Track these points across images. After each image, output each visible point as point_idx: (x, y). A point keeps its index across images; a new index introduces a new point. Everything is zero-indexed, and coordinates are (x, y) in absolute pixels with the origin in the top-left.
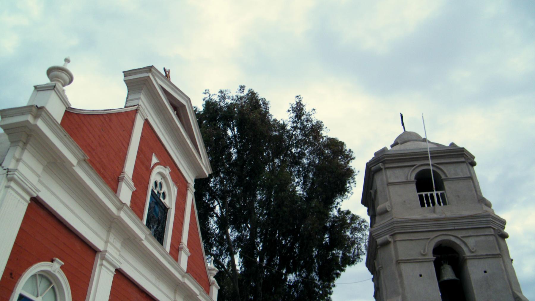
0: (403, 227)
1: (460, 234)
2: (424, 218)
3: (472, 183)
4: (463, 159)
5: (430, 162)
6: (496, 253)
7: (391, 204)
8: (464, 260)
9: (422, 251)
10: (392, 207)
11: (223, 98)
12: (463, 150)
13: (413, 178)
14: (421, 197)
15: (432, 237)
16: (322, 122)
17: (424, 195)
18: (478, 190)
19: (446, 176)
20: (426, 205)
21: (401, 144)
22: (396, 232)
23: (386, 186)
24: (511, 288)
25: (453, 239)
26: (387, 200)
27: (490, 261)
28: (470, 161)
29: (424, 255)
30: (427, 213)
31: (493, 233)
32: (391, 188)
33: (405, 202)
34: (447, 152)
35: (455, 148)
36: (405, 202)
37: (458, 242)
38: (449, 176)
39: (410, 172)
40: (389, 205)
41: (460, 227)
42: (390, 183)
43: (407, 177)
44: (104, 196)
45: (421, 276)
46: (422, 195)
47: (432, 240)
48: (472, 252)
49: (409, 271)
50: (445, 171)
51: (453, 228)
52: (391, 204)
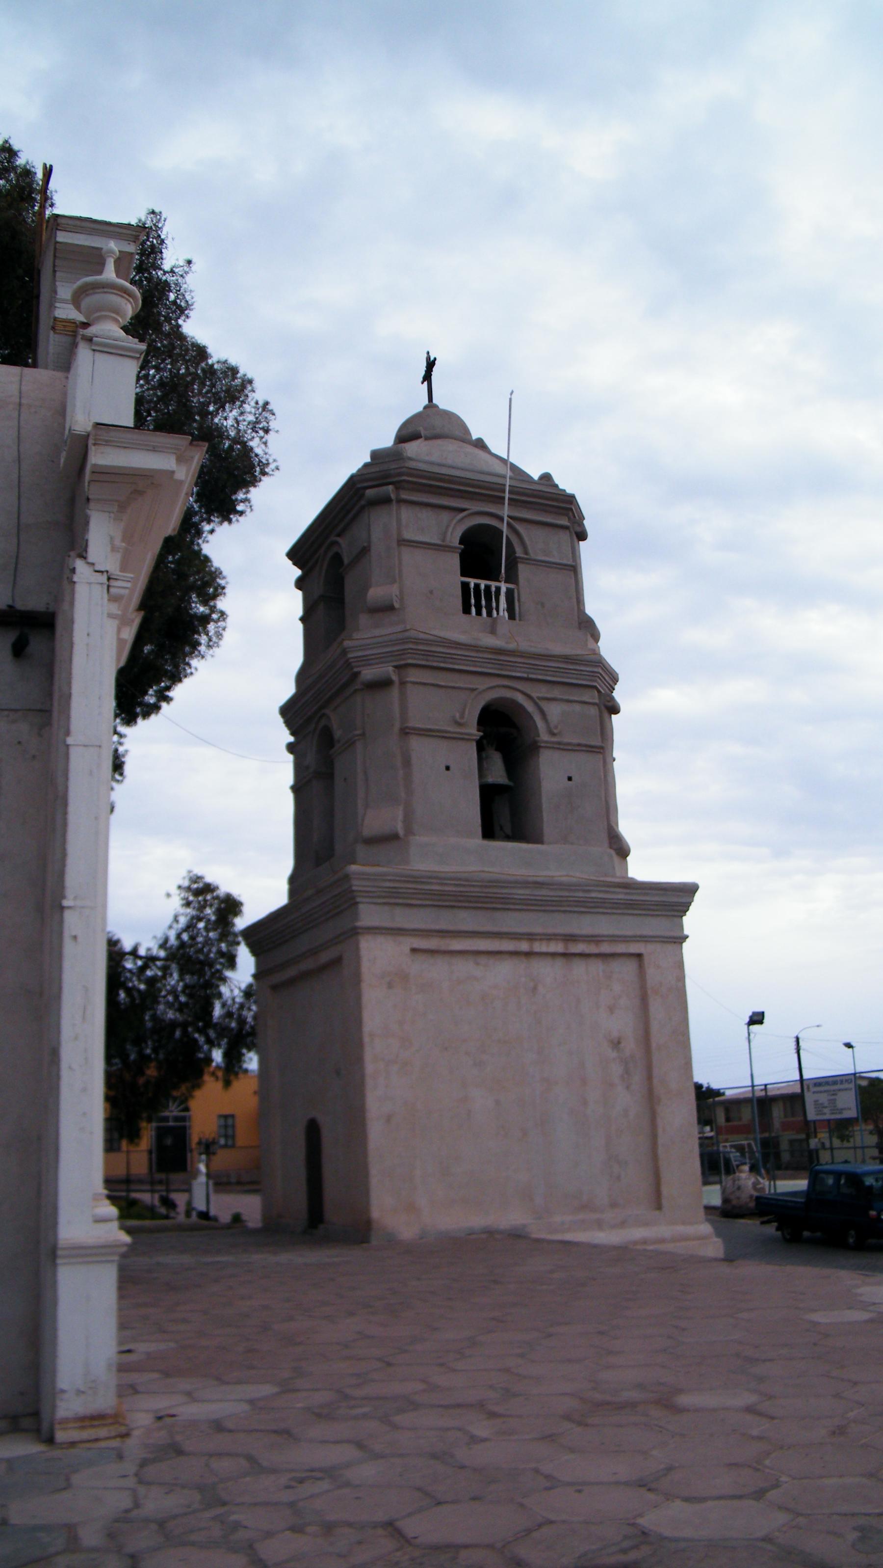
0: (428, 654)
1: (538, 691)
2: (473, 642)
5: (506, 511)
7: (401, 592)
8: (535, 748)
9: (458, 715)
10: (401, 599)
12: (571, 499)
13: (456, 542)
14: (465, 586)
15: (481, 687)
17: (472, 585)
19: (526, 553)
20: (473, 610)
22: (410, 661)
23: (394, 544)
25: (520, 699)
27: (583, 757)
31: (597, 701)
33: (431, 592)
34: (539, 497)
36: (431, 592)
38: (532, 555)
39: (455, 521)
41: (540, 677)
42: (404, 540)
44: (596, 1241)
45: (448, 768)
47: (480, 693)
49: (427, 755)
51: (525, 675)
52: (401, 592)
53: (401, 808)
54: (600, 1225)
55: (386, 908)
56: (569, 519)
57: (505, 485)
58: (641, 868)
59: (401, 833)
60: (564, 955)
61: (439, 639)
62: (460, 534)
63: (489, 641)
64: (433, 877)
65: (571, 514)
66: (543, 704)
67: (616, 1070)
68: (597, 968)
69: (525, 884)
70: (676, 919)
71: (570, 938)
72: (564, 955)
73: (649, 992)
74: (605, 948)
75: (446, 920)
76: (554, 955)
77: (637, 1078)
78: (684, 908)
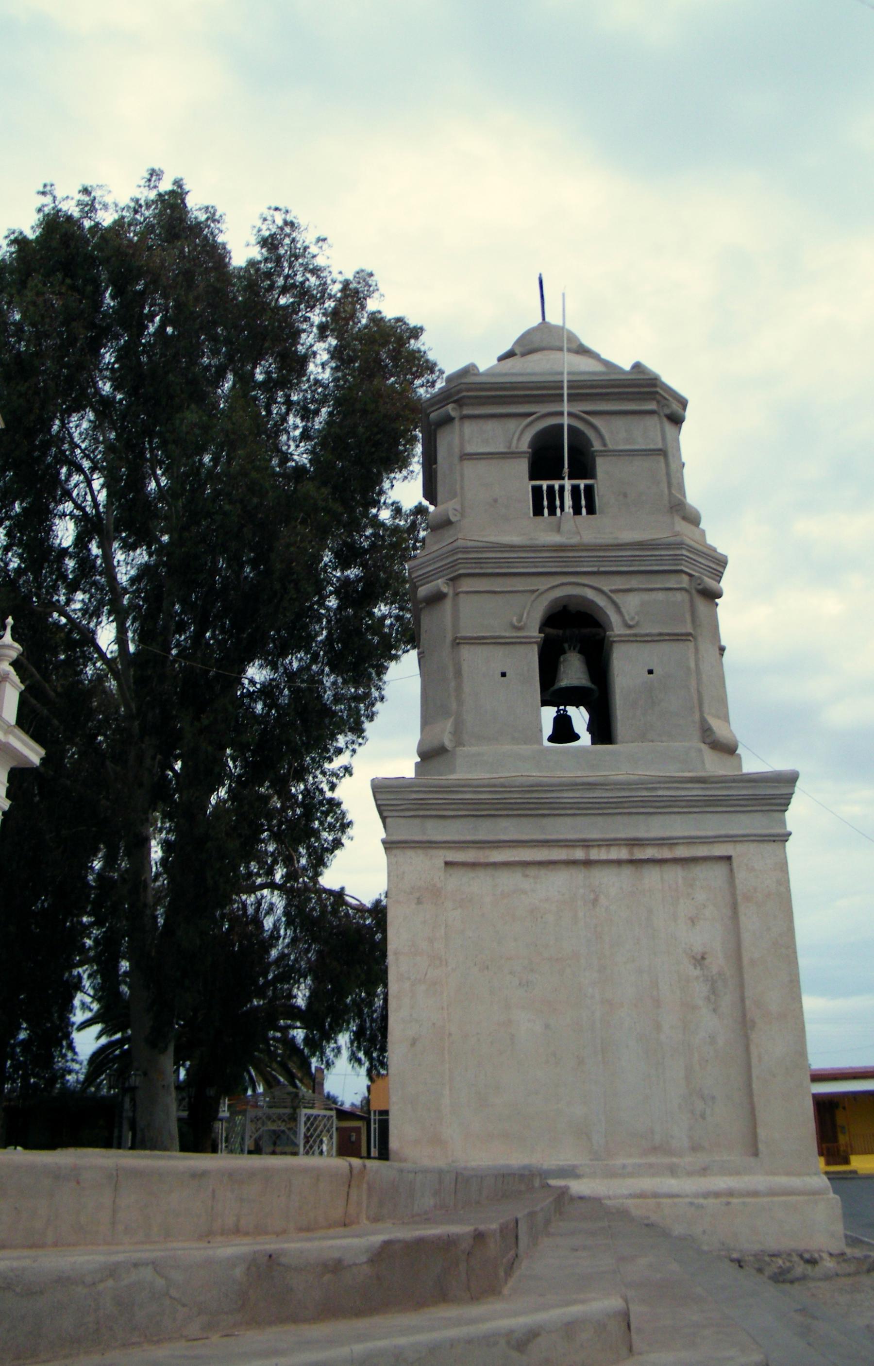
0: (479, 562)
1: (606, 584)
2: (528, 543)
3: (663, 465)
4: (652, 406)
6: (683, 631)
9: (515, 620)
11: (89, 208)
13: (524, 445)
14: (537, 491)
15: (542, 588)
16: (371, 275)
17: (545, 488)
18: (674, 481)
19: (605, 445)
20: (546, 511)
21: (523, 355)
22: (461, 571)
23: (456, 460)
24: (701, 711)
25: (590, 594)
26: (455, 495)
27: (665, 648)
28: (668, 411)
29: (519, 629)
30: (543, 533)
32: (468, 466)
33: (496, 501)
35: (642, 377)
36: (496, 501)
37: (601, 601)
38: (611, 446)
40: (458, 507)
43: (510, 443)
45: (504, 675)
46: (540, 487)
47: (542, 593)
48: (630, 627)
50: (603, 431)
51: (595, 569)
53: (452, 720)
54: (673, 1171)
55: (417, 821)
56: (658, 402)
57: (562, 382)
58: (753, 762)
59: (448, 744)
60: (632, 862)
61: (491, 545)
62: (529, 439)
63: (555, 539)
64: (475, 786)
65: (657, 396)
66: (614, 596)
67: (700, 990)
68: (675, 875)
69: (574, 786)
70: (776, 815)
71: (634, 843)
72: (632, 862)
73: (739, 898)
74: (682, 852)
75: (485, 830)
76: (619, 862)
77: (727, 1000)
78: (783, 802)
